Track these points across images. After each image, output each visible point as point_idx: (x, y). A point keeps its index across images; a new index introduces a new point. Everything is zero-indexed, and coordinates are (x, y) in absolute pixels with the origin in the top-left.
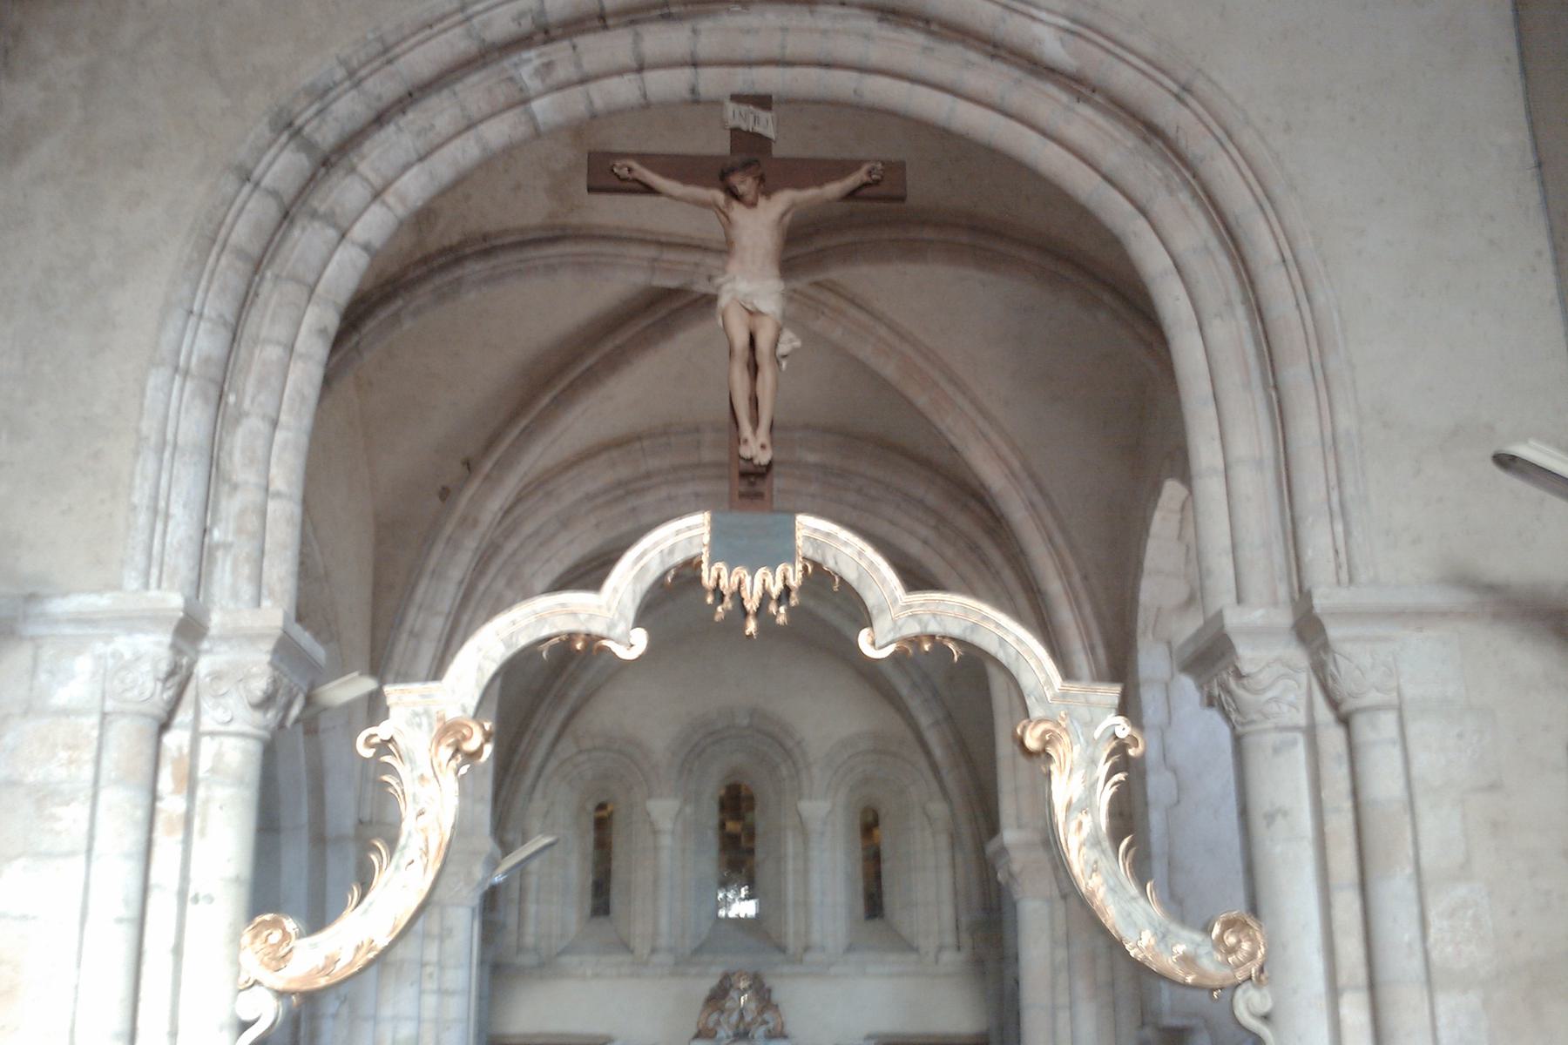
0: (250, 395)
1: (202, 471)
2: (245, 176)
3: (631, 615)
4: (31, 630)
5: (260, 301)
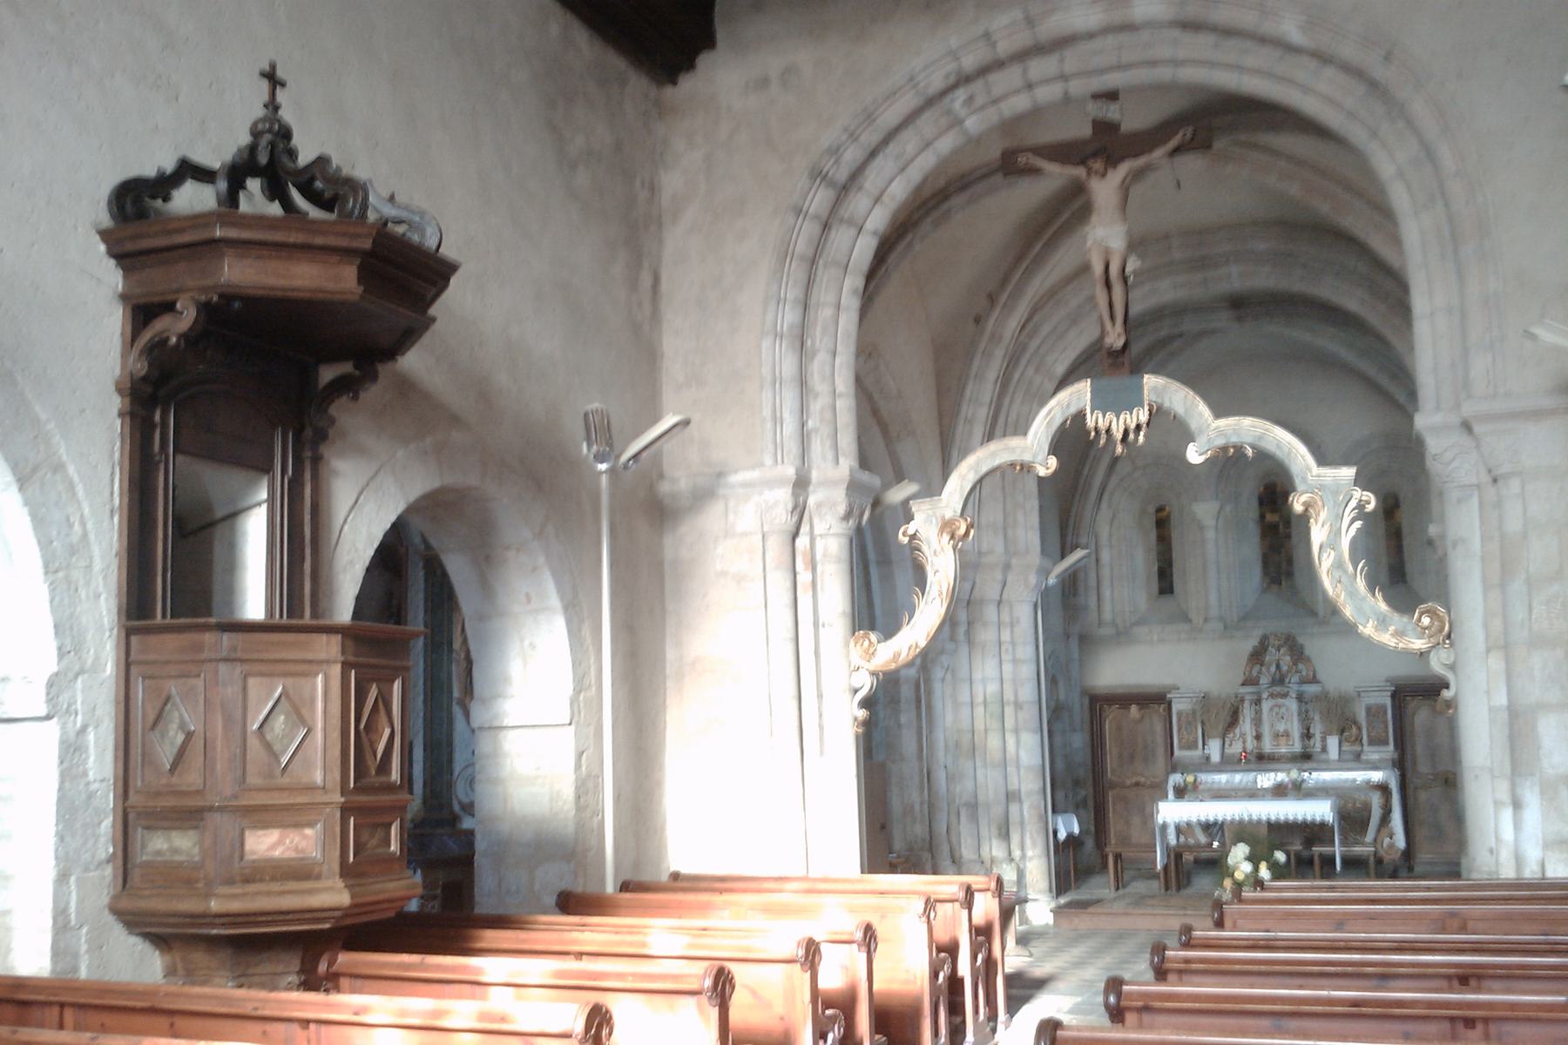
0: (819, 340)
1: (797, 391)
2: (798, 211)
3: (1046, 448)
4: (721, 491)
5: (818, 280)
